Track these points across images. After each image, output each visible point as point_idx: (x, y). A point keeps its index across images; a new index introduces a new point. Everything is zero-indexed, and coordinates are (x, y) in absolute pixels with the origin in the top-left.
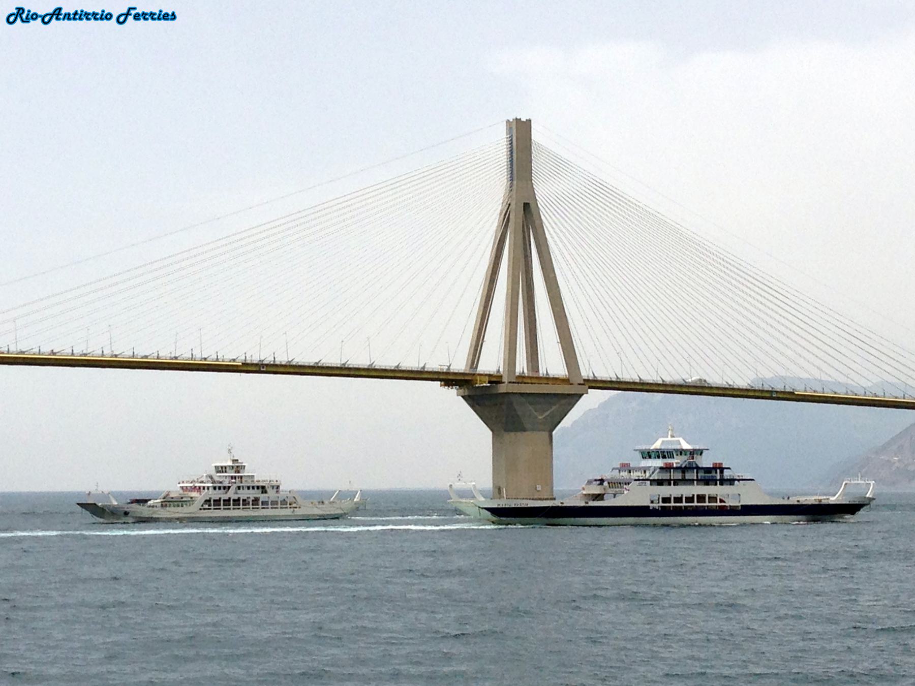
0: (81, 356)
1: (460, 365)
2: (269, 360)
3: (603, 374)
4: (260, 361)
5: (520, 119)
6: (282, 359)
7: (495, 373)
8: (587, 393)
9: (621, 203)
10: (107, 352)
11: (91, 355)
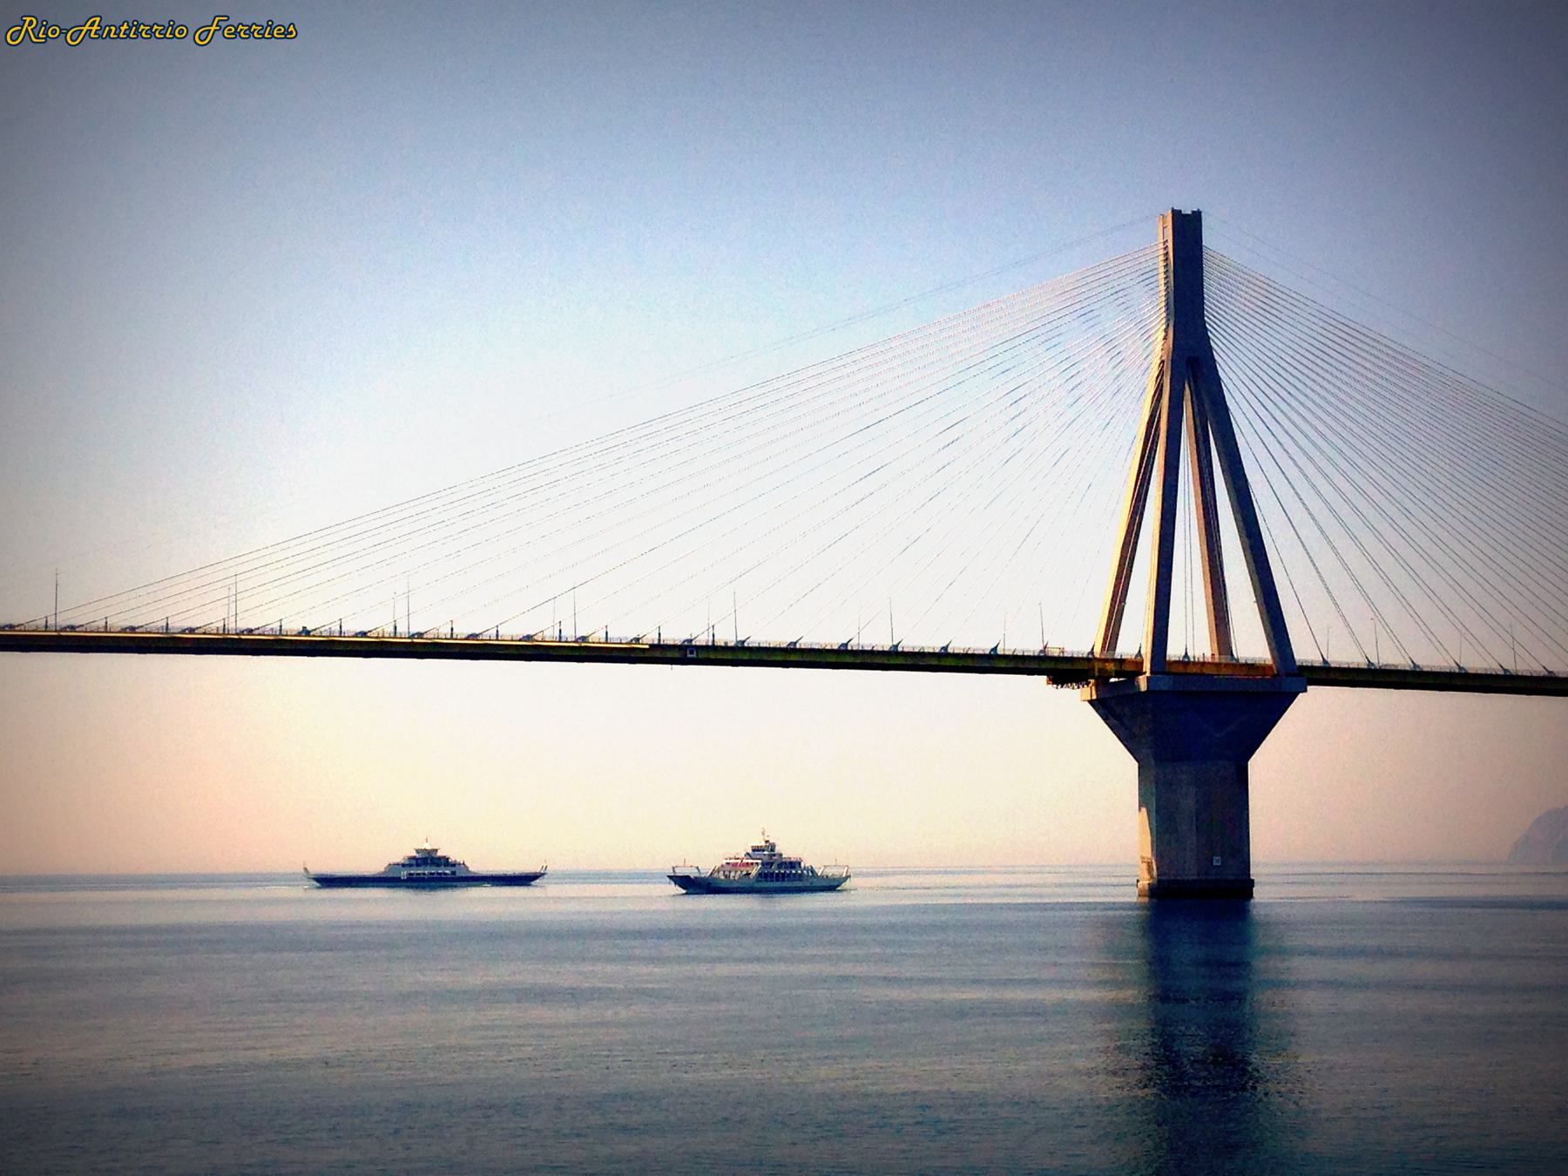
0: (356, 635)
1: (1082, 640)
2: (703, 639)
3: (1344, 655)
4: (738, 642)
5: (1181, 211)
6: (726, 637)
7: (1133, 657)
8: (1305, 691)
9: (1366, 391)
10: (231, 626)
11: (202, 631)
